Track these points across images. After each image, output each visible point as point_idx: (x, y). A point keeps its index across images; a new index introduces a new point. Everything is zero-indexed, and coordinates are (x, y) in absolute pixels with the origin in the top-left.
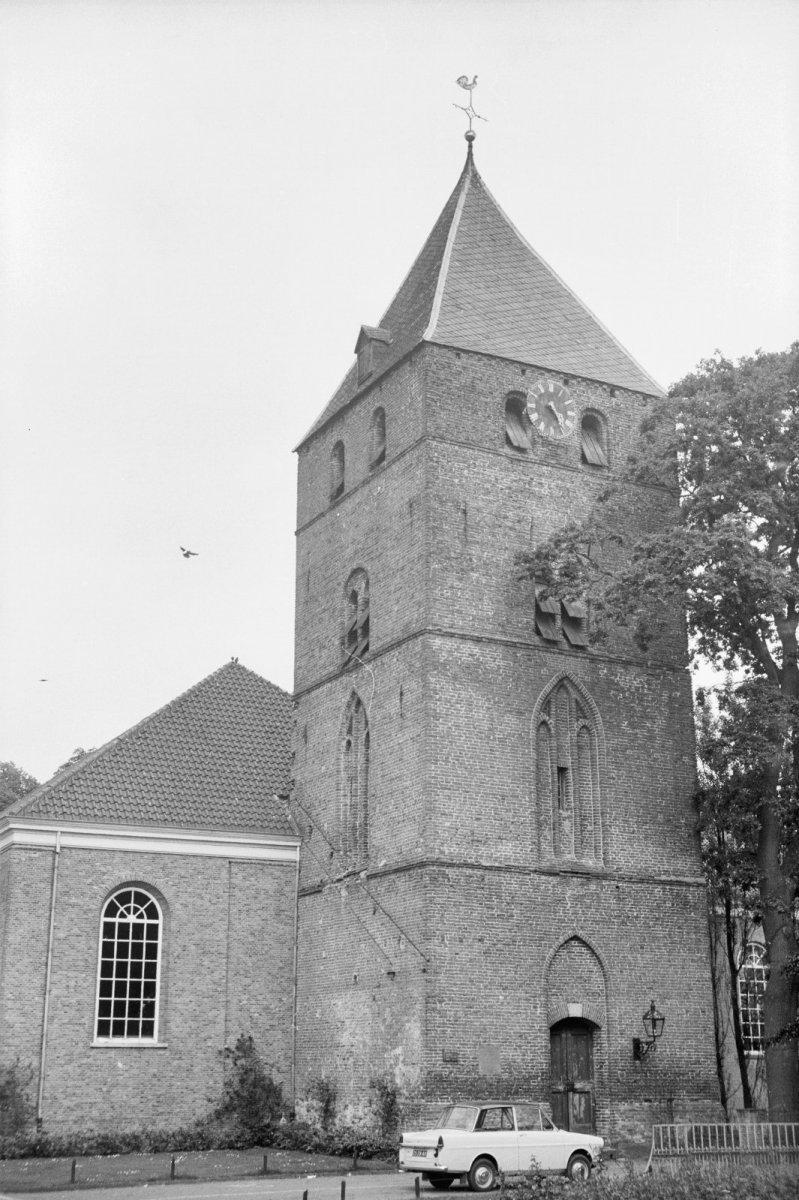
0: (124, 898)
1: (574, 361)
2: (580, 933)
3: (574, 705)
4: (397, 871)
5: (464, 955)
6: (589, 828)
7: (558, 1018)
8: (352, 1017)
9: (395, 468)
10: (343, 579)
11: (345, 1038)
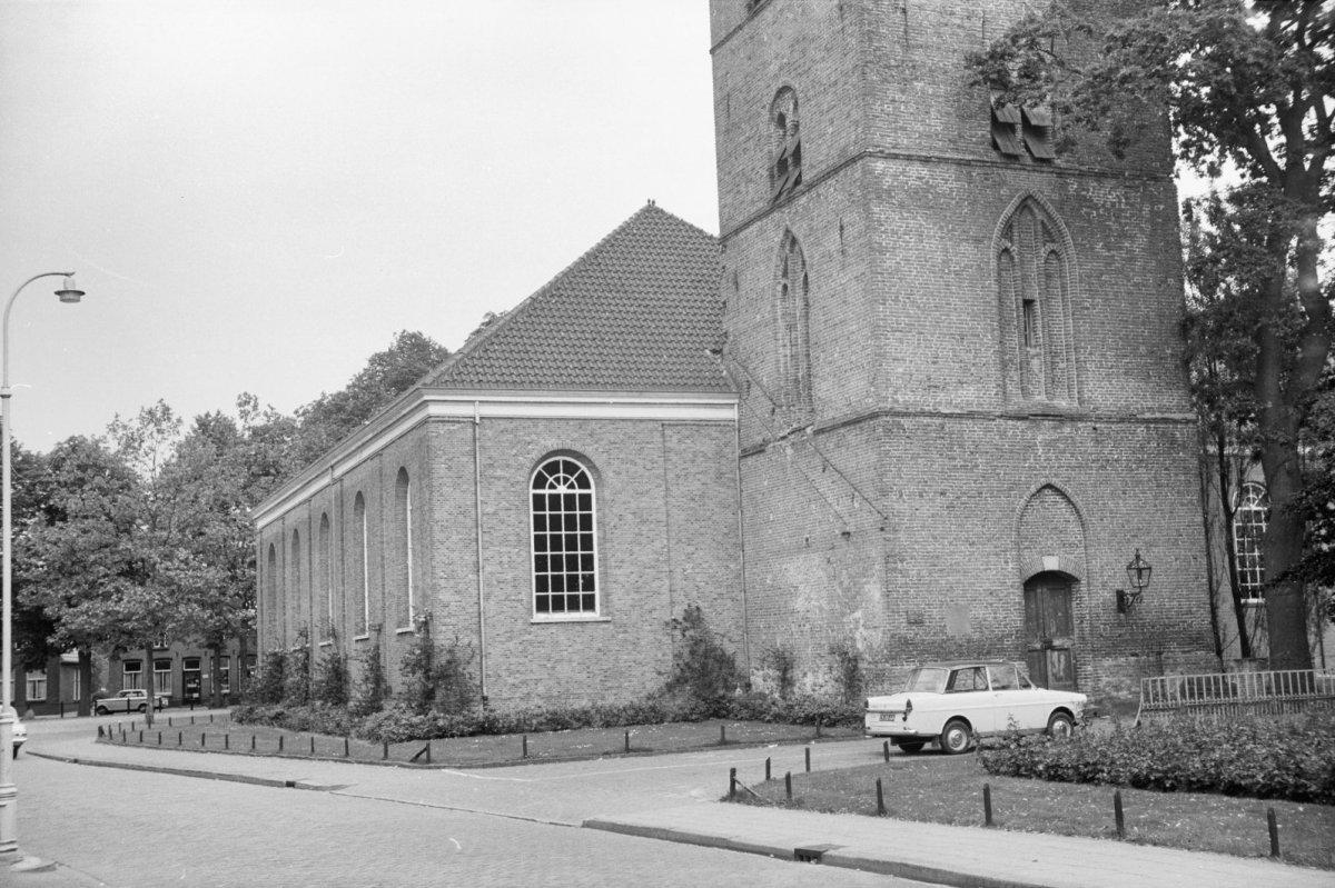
0: (553, 468)
2: (1054, 481)
3: (1039, 227)
4: (845, 424)
5: (926, 509)
6: (1062, 365)
7: (1032, 573)
10: (768, 100)
11: (799, 604)
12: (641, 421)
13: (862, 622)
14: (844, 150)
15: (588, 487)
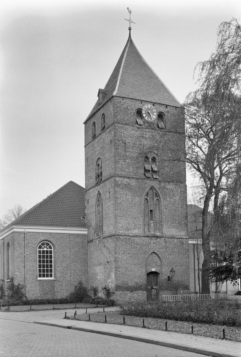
0: (43, 244)
1: (156, 98)
2: (155, 251)
3: (154, 193)
4: (109, 237)
5: (125, 257)
6: (158, 225)
8: (100, 272)
9: (107, 131)
10: (96, 160)
11: (98, 277)
12: (65, 234)
13: (110, 282)
14: (110, 174)
15: (52, 249)
